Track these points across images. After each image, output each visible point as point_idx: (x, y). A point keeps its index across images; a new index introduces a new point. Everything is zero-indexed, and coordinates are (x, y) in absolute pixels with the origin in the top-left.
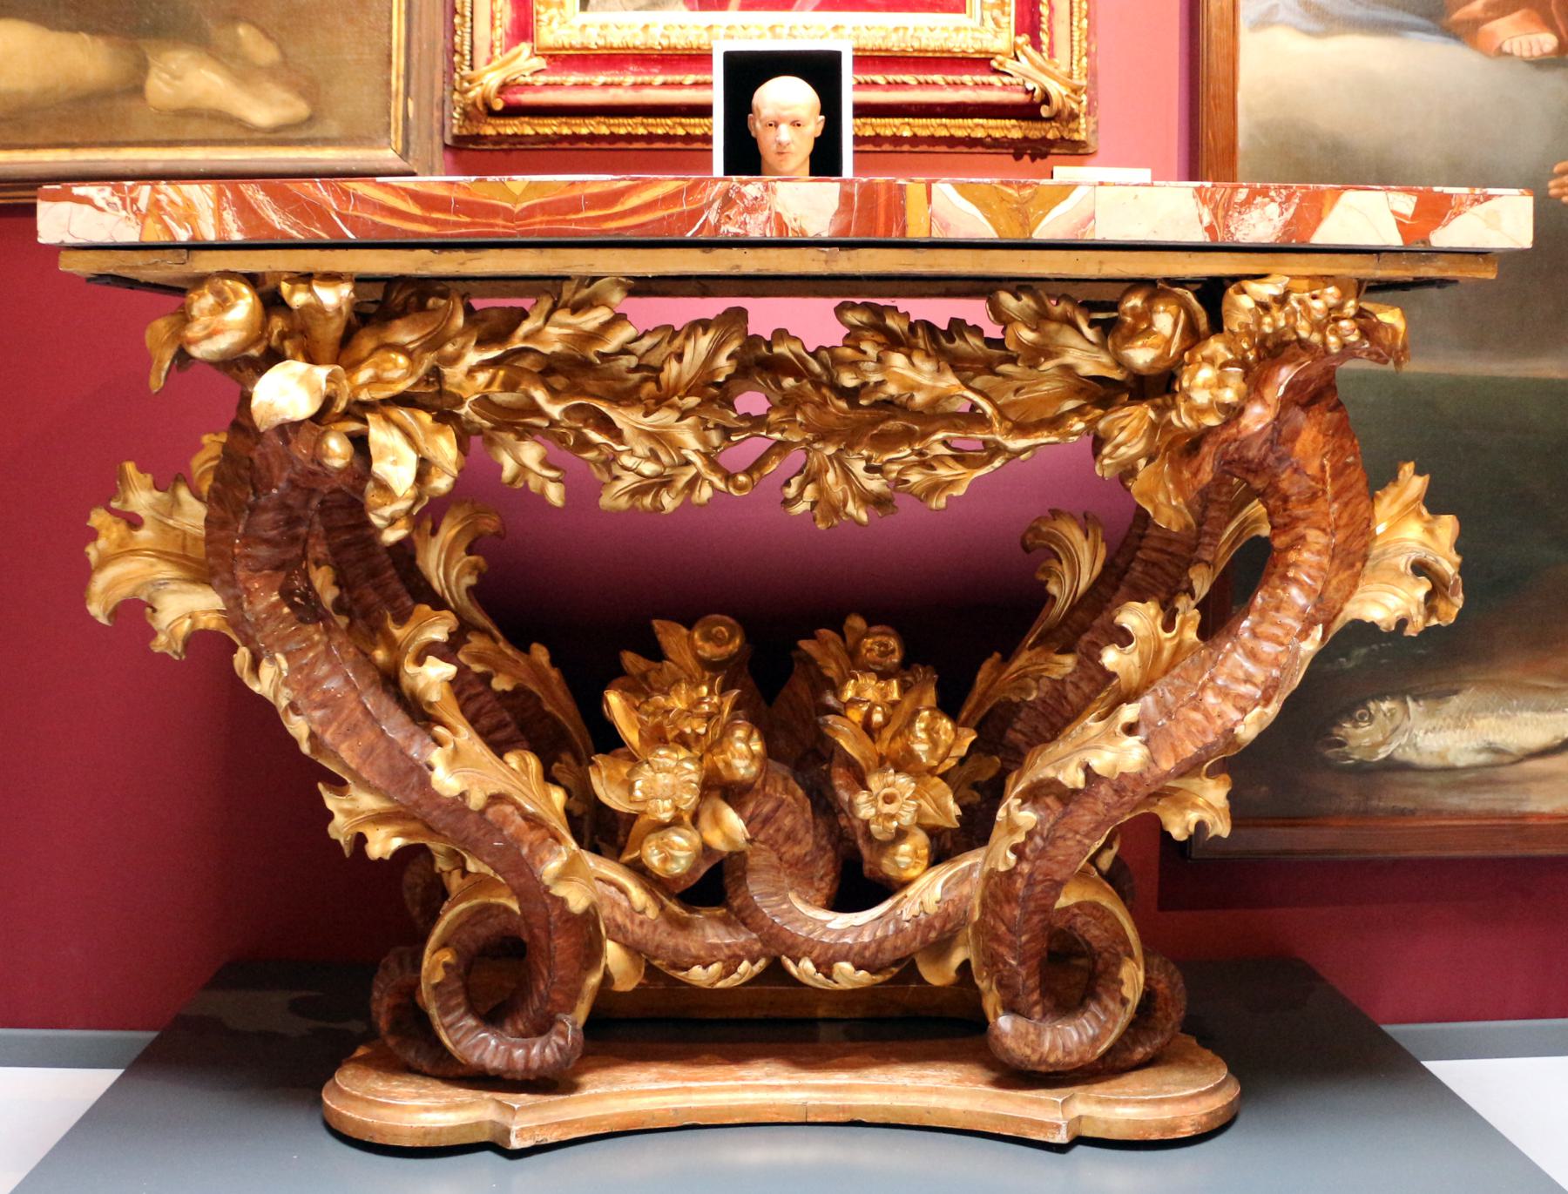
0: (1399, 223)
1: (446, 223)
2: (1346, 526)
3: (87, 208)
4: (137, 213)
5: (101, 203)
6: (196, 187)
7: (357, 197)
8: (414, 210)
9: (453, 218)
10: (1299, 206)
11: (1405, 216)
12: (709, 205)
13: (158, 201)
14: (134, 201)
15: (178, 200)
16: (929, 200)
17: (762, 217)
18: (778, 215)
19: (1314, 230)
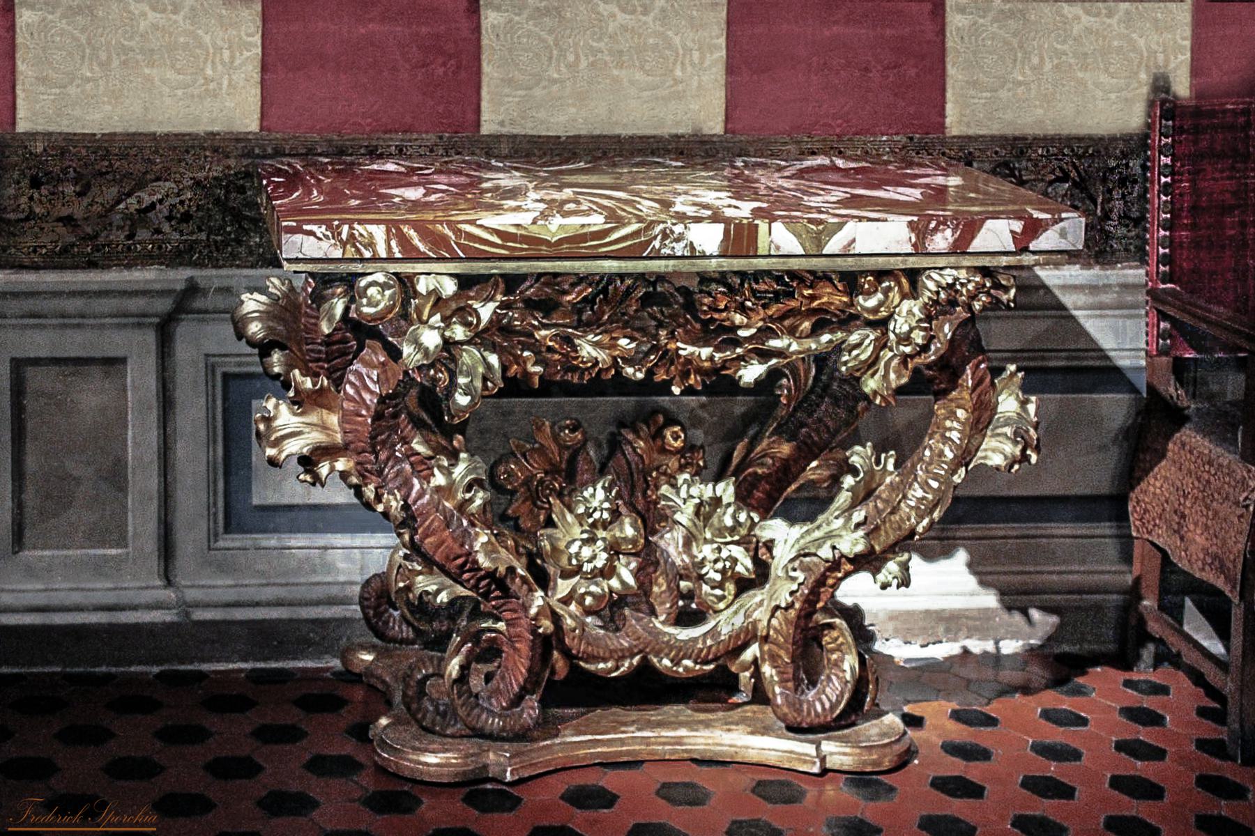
0: (1014, 237)
1: (515, 249)
2: (426, 464)
3: (312, 238)
4: (341, 241)
5: (320, 235)
6: (375, 226)
7: (466, 232)
8: (499, 241)
9: (518, 246)
10: (962, 230)
11: (1016, 233)
12: (655, 238)
13: (353, 234)
14: (340, 234)
15: (365, 234)
16: (770, 234)
17: (682, 244)
18: (691, 243)
19: (969, 244)
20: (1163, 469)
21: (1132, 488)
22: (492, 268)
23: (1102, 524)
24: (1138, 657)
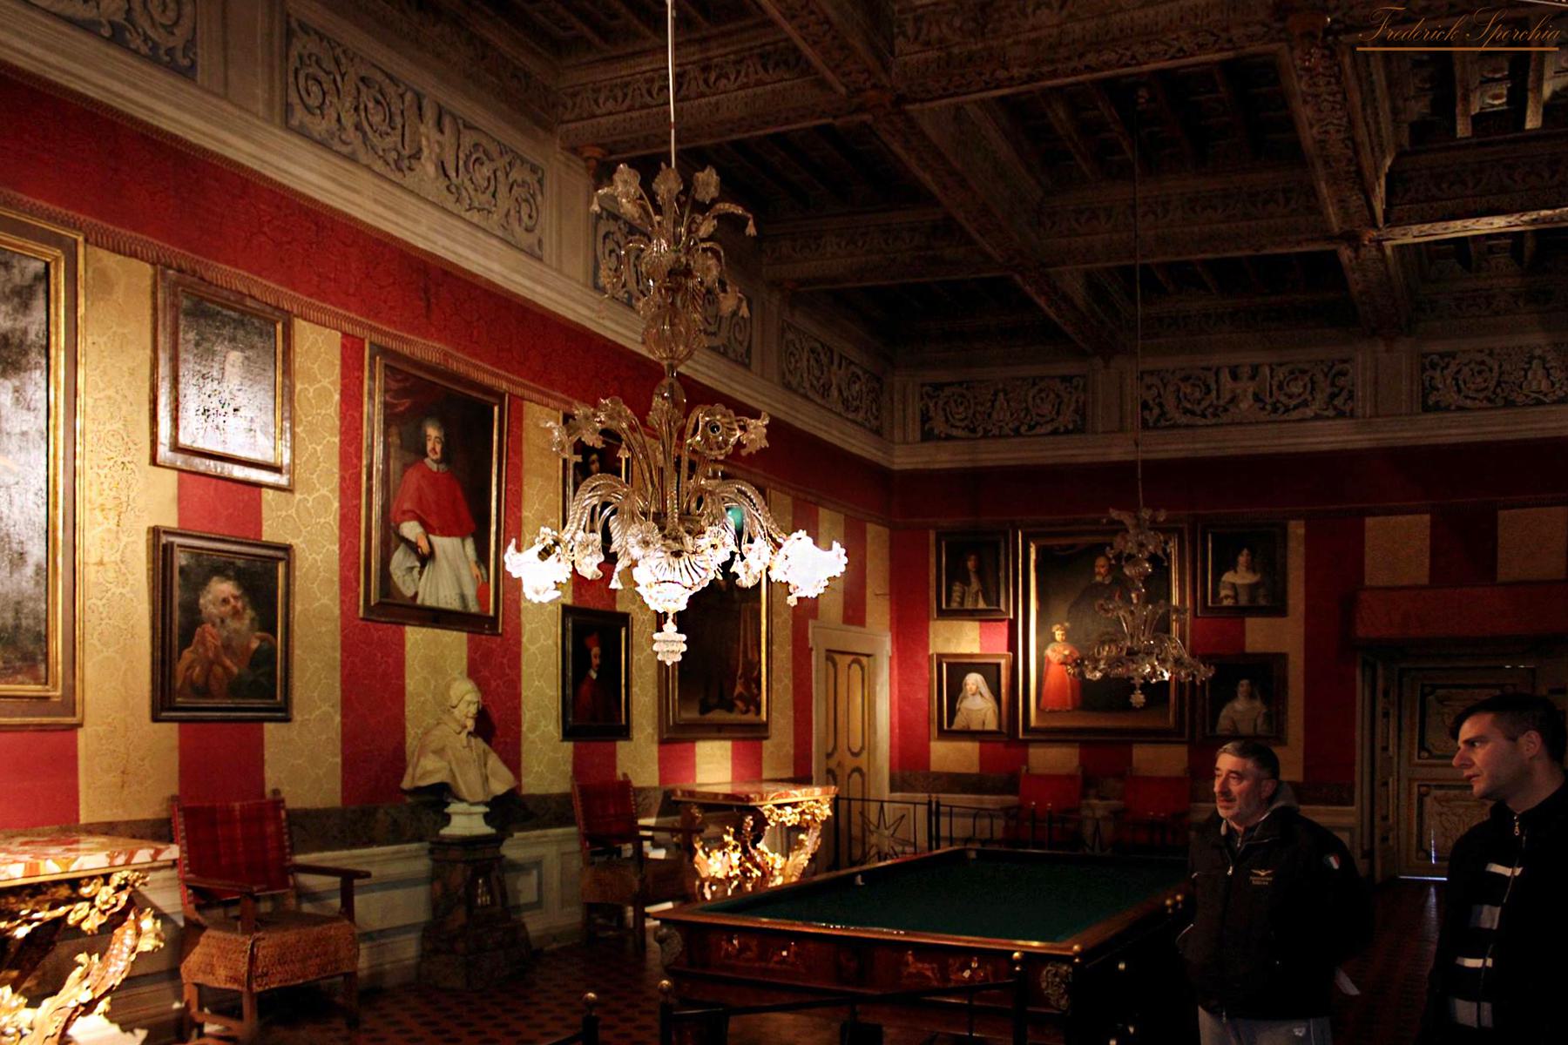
20: (198, 949)
21: (182, 962)
22: (887, 933)
23: (1458, 75)
24: (190, 1036)
